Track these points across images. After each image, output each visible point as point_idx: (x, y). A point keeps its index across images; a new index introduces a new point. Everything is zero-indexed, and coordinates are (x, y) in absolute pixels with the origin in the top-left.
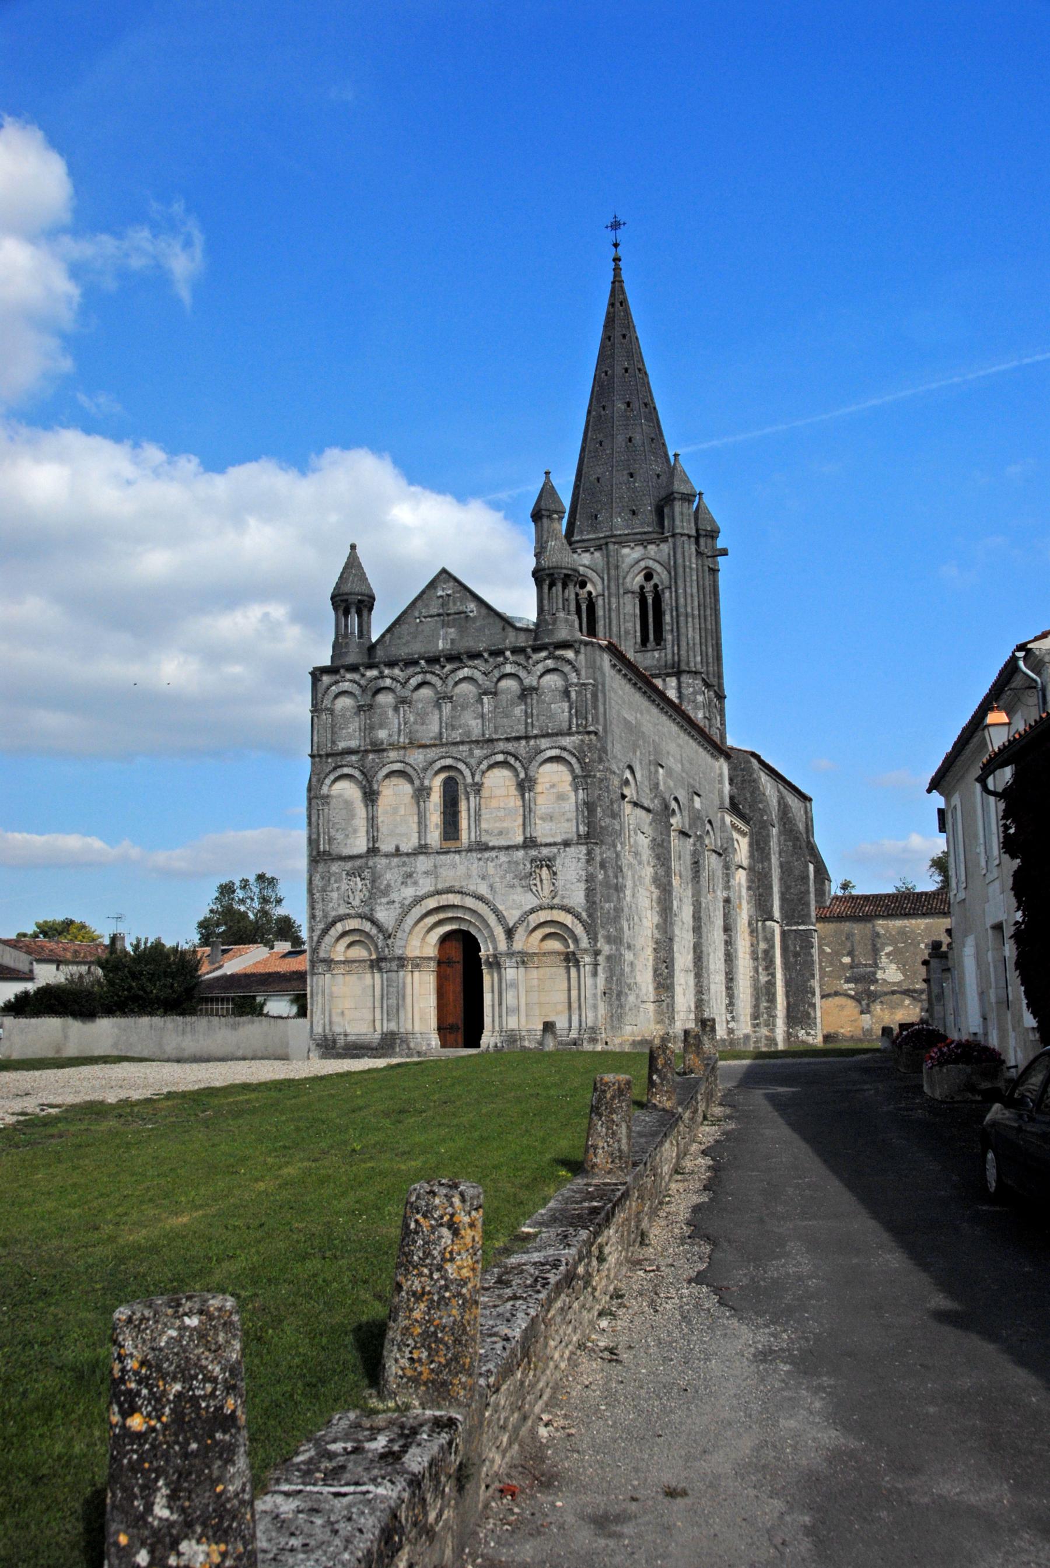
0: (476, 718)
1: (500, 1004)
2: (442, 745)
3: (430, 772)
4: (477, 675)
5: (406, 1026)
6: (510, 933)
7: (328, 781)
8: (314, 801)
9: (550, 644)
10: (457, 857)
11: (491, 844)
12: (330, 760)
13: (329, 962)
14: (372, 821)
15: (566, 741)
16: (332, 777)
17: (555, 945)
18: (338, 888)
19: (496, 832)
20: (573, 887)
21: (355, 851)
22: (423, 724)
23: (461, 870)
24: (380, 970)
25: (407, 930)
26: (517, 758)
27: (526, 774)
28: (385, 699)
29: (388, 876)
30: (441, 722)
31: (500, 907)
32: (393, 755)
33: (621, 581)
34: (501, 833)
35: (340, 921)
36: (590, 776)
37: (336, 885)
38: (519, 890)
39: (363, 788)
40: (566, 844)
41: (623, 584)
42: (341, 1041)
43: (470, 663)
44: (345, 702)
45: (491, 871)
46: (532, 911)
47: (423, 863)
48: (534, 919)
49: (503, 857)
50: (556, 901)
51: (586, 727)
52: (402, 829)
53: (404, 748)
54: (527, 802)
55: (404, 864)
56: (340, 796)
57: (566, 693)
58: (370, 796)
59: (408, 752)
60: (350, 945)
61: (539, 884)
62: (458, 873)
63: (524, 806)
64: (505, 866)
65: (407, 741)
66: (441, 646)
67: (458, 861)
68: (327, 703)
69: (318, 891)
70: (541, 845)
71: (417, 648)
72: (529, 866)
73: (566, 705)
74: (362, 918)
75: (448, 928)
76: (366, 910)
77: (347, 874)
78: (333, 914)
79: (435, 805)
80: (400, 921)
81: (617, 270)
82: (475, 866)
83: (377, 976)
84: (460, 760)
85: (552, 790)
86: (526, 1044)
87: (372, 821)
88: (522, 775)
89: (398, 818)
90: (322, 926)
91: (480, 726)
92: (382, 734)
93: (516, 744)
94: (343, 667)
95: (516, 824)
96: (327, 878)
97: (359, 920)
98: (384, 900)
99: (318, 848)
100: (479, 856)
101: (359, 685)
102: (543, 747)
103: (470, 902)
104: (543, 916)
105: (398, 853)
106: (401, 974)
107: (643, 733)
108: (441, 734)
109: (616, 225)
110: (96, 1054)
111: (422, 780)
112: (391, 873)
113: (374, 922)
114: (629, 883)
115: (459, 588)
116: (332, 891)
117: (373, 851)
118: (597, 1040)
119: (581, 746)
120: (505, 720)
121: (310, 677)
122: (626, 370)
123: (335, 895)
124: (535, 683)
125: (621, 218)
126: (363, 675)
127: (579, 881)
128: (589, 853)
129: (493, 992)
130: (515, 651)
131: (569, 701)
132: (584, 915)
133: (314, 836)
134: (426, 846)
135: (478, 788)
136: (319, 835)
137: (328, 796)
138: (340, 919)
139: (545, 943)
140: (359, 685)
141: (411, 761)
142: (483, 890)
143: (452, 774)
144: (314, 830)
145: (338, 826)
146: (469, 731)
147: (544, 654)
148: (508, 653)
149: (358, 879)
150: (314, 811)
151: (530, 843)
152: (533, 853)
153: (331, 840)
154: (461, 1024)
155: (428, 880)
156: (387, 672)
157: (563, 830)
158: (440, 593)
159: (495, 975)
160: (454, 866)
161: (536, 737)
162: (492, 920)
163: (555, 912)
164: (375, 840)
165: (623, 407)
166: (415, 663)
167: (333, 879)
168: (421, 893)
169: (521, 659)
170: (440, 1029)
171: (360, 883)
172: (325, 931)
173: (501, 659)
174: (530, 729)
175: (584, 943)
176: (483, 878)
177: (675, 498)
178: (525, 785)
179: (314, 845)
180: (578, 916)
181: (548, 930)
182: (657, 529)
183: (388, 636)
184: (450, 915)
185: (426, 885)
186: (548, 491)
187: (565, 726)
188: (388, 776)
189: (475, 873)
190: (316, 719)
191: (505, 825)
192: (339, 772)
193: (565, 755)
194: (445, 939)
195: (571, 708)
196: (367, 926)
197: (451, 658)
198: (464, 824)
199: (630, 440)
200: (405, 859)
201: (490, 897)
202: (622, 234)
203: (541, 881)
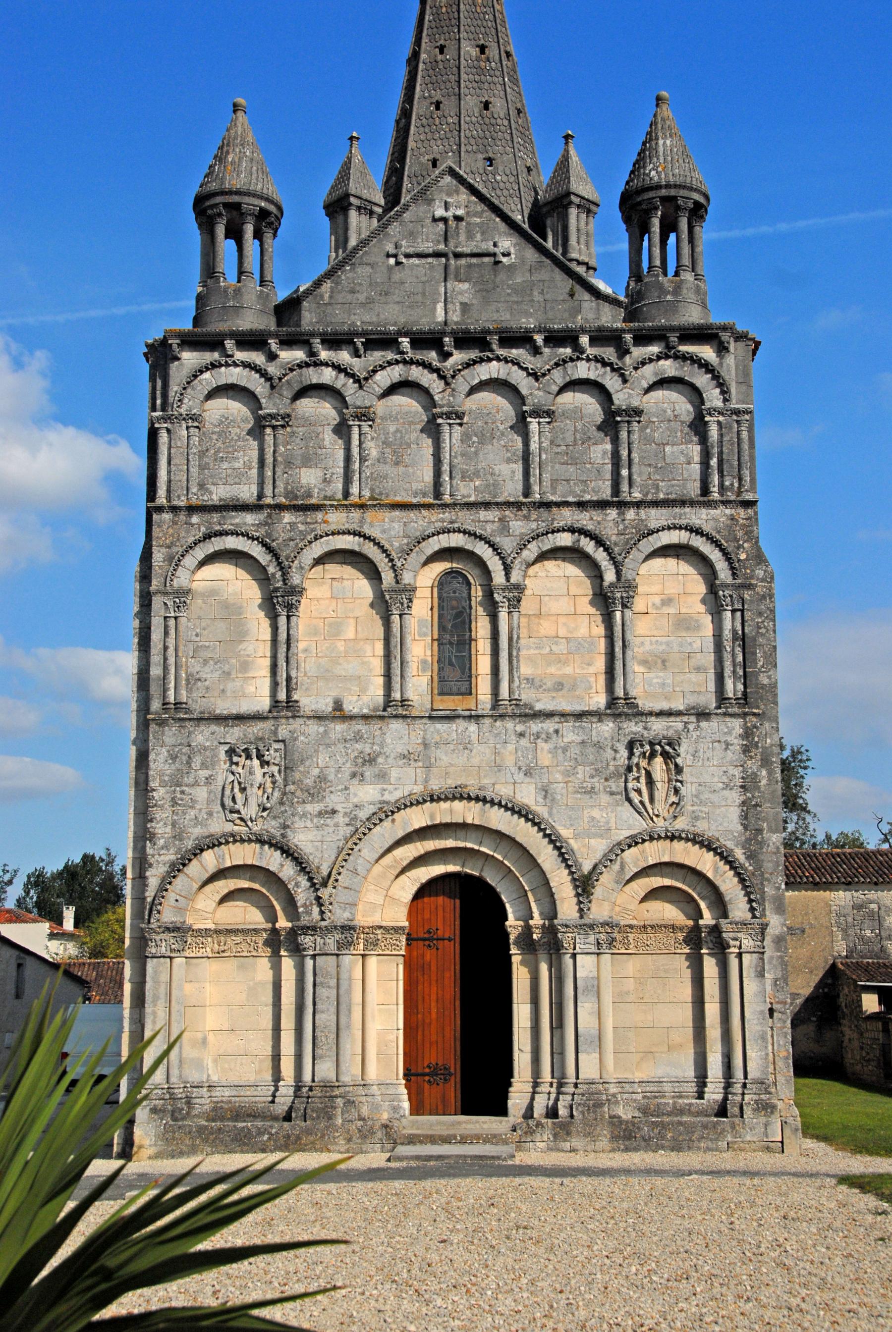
0: (509, 461)
1: (558, 1025)
3: (416, 558)
4: (518, 377)
7: (190, 561)
10: (473, 727)
11: (538, 707)
12: (195, 519)
16: (200, 553)
17: (670, 912)
18: (209, 780)
19: (549, 684)
20: (714, 798)
21: (245, 707)
22: (397, 464)
26: (600, 542)
29: (323, 759)
32: (336, 519)
34: (559, 686)
37: (204, 773)
38: (605, 798)
42: (203, 1102)
43: (502, 352)
45: (545, 759)
46: (634, 841)
48: (634, 859)
49: (570, 733)
50: (681, 824)
51: (739, 493)
52: (350, 667)
53: (362, 506)
55: (358, 737)
57: (699, 426)
60: (653, 894)
62: (476, 761)
64: (575, 750)
67: (474, 737)
69: (163, 784)
73: (695, 450)
75: (426, 873)
76: (271, 827)
77: (231, 752)
78: (197, 831)
79: (421, 622)
80: (346, 852)
82: (511, 747)
84: (481, 538)
85: (666, 610)
89: (341, 646)
93: (597, 515)
94: (233, 335)
95: (592, 670)
98: (313, 808)
100: (520, 728)
102: (653, 525)
103: (498, 819)
104: (656, 852)
106: (346, 960)
113: (287, 852)
115: (480, 207)
116: (196, 784)
118: (774, 1107)
119: (730, 528)
120: (571, 469)
123: (201, 793)
127: (727, 786)
128: (748, 734)
130: (600, 337)
132: (739, 855)
136: (165, 668)
138: (214, 843)
139: (646, 905)
140: (263, 374)
142: (528, 796)
145: (208, 654)
146: (496, 485)
149: (256, 762)
152: (633, 727)
154: (454, 1065)
155: (411, 771)
156: (324, 355)
157: (687, 688)
158: (440, 212)
159: (544, 968)
160: (467, 746)
161: (638, 504)
163: (678, 845)
165: (474, 52)
167: (197, 761)
168: (392, 797)
169: (609, 353)
171: (259, 771)
172: (178, 867)
174: (625, 487)
175: (739, 909)
176: (528, 773)
177: (571, 203)
181: (658, 881)
183: (327, 286)
184: (450, 843)
188: (320, 561)
189: (510, 761)
191: (568, 670)
192: (218, 544)
193: (698, 542)
194: (425, 891)
196: (273, 860)
197: (464, 340)
199: (486, 105)
203: (650, 782)
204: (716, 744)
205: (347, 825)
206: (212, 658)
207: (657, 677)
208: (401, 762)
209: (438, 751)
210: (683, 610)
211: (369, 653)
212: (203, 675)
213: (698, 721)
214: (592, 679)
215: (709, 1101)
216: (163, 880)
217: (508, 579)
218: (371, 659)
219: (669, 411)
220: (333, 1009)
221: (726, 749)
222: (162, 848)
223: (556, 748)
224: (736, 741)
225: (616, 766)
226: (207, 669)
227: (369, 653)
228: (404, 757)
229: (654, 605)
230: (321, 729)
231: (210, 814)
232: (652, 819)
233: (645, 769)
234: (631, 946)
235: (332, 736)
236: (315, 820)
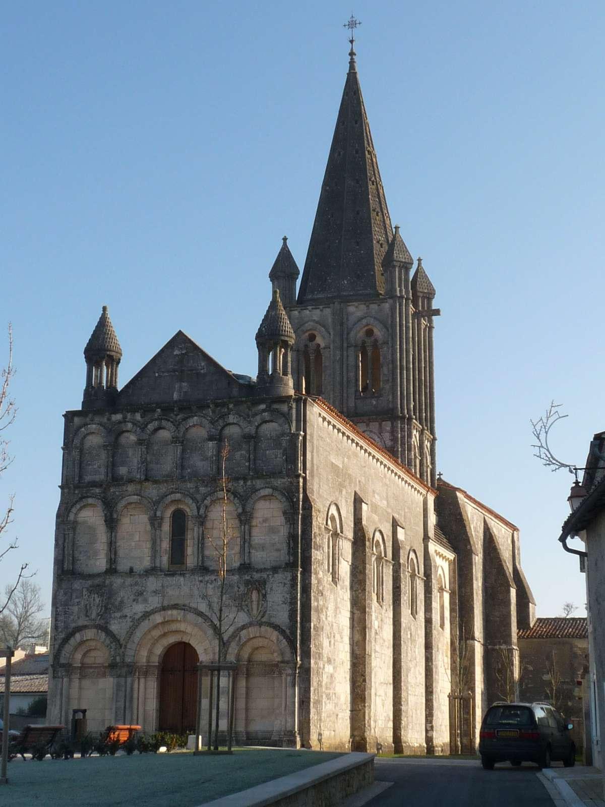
0: (203, 460)
7: (74, 510)
14: (112, 545)
18: (78, 603)
21: (95, 571)
22: (157, 463)
23: (185, 590)
29: (122, 594)
33: (345, 336)
37: (77, 600)
40: (275, 569)
41: (347, 339)
46: (243, 627)
47: (152, 583)
50: (264, 620)
55: (136, 584)
58: (111, 523)
66: (176, 396)
69: (61, 605)
78: (73, 625)
81: (352, 63)
90: (62, 636)
92: (123, 471)
97: (95, 630)
98: (118, 615)
106: (129, 680)
107: (349, 475)
109: (352, 24)
110: (341, 511)
112: (123, 589)
114: (331, 606)
116: (73, 605)
117: (112, 570)
121: (63, 419)
125: (358, 18)
132: (288, 631)
147: (263, 406)
151: (245, 567)
156: (129, 415)
160: (179, 587)
178: (245, 518)
185: (154, 602)
192: (85, 501)
202: (357, 32)
204: (280, 584)
205: (131, 622)
206: (83, 551)
207: (259, 555)
208: (153, 594)
209: (168, 589)
210: (271, 524)
211: (144, 547)
212: (80, 558)
213: (273, 574)
214: (233, 556)
215: (273, 740)
216: (59, 646)
217: (198, 513)
218: (145, 549)
219: (268, 435)
220: (123, 700)
221: (284, 586)
222: (60, 632)
223: (215, 587)
224: (288, 582)
225: (239, 595)
226: (81, 555)
227: (144, 547)
228: (154, 592)
229: (260, 522)
230: (122, 581)
231: (78, 618)
235: (126, 584)
236: (119, 620)
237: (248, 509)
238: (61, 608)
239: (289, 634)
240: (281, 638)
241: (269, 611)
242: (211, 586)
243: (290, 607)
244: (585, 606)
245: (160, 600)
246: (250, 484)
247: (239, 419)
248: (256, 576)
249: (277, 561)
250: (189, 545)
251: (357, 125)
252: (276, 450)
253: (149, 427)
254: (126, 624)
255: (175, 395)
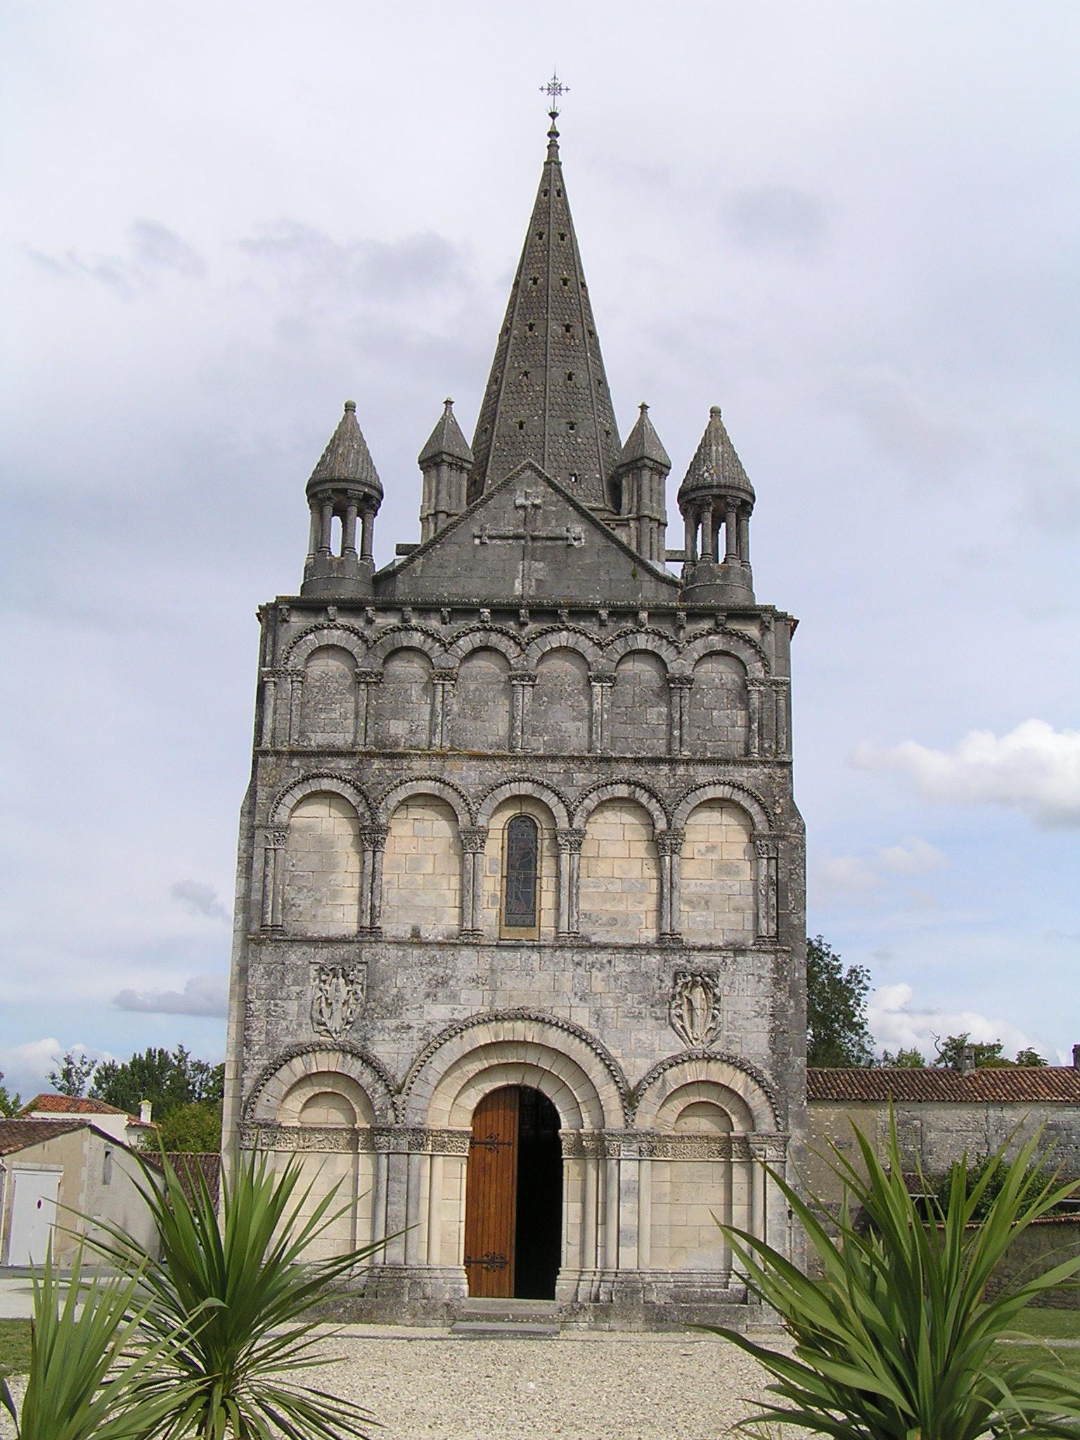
0: (574, 719)
2: (516, 758)
3: (489, 805)
4: (584, 645)
5: (418, 1256)
6: (630, 1099)
7: (290, 800)
8: (260, 834)
9: (721, 609)
10: (535, 956)
12: (295, 763)
13: (272, 1128)
14: (370, 878)
15: (742, 775)
16: (298, 794)
18: (300, 995)
21: (333, 931)
22: (475, 719)
24: (373, 1148)
25: (433, 1079)
26: (652, 794)
27: (669, 822)
28: (408, 670)
29: (400, 980)
30: (513, 718)
31: (613, 1052)
32: (419, 766)
35: (301, 1054)
36: (783, 838)
37: (298, 989)
38: (650, 1023)
39: (356, 817)
40: (739, 950)
43: (571, 624)
44: (331, 665)
45: (598, 986)
46: (675, 1062)
47: (467, 962)
48: (674, 1077)
49: (622, 964)
50: (716, 1047)
54: (667, 872)
55: (433, 962)
56: (309, 828)
59: (449, 764)
61: (686, 1016)
62: (537, 986)
63: (661, 880)
64: (625, 979)
65: (447, 744)
67: (536, 965)
68: (296, 661)
70: (694, 949)
71: (474, 588)
72: (669, 982)
73: (740, 715)
74: (344, 1051)
76: (354, 1038)
78: (289, 1040)
79: (492, 861)
80: (420, 1063)
81: (553, 147)
82: (568, 974)
83: (365, 1163)
84: (547, 787)
85: (710, 856)
86: (653, 1297)
87: (370, 878)
88: (661, 825)
91: (584, 732)
92: (397, 728)
93: (651, 770)
94: (335, 602)
95: (643, 908)
96: (279, 974)
97: (339, 1055)
98: (391, 1023)
99: (262, 918)
100: (577, 958)
101: (361, 637)
102: (700, 780)
103: (555, 1038)
104: (693, 1072)
105: (416, 939)
106: (416, 1159)
108: (511, 738)
109: (555, 89)
111: (473, 817)
113: (367, 1061)
116: (288, 998)
117: (370, 932)
122: (565, 282)
123: (293, 1007)
124: (688, 672)
126: (370, 622)
127: (758, 1014)
128: (778, 968)
129: (584, 1202)
130: (659, 613)
131: (747, 707)
132: (767, 1074)
133: (256, 896)
134: (474, 932)
135: (577, 839)
136: (265, 894)
137: (288, 827)
140: (361, 637)
141: (454, 780)
142: (582, 1018)
143: (528, 810)
144: (257, 885)
147: (706, 625)
148: (644, 615)
149: (342, 980)
150: (259, 852)
151: (668, 942)
152: (678, 960)
153: (287, 906)
154: (510, 1255)
157: (726, 926)
158: (520, 501)
159: (592, 1173)
160: (530, 973)
161: (688, 762)
162: (597, 1072)
164: (374, 913)
165: (561, 330)
166: (469, 611)
167: (290, 978)
169: (666, 629)
170: (467, 1262)
171: (344, 989)
172: (270, 1071)
173: (630, 625)
175: (766, 1123)
179: (255, 913)
180: (755, 1076)
182: (610, 507)
185: (473, 1002)
186: (447, 427)
187: (737, 750)
188: (404, 803)
189: (567, 986)
190: (270, 689)
191: (621, 908)
192: (314, 786)
193: (739, 797)
195: (750, 720)
196: (354, 1068)
197: (538, 612)
198: (546, 900)
200: (436, 953)
201: (593, 1031)
202: (561, 103)
203: (691, 1009)
206: (305, 887)
207: (700, 916)
213: (735, 956)
214: (643, 916)
224: (767, 975)
225: (661, 994)
226: (301, 896)
230: (401, 953)
231: (300, 1025)
232: (691, 1042)
233: (687, 998)
234: (669, 1154)
237: (678, 824)
238: (258, 1003)
239: (769, 1078)
240: (751, 1083)
241: (728, 1031)
242: (600, 975)
243: (773, 1025)
244: (172, 1050)
245: (486, 997)
246: (683, 773)
247: (659, 642)
248: (699, 959)
249: (737, 931)
250: (545, 888)
251: (564, 243)
252: (734, 711)
253: (461, 642)
254: (410, 1046)
255: (517, 585)
